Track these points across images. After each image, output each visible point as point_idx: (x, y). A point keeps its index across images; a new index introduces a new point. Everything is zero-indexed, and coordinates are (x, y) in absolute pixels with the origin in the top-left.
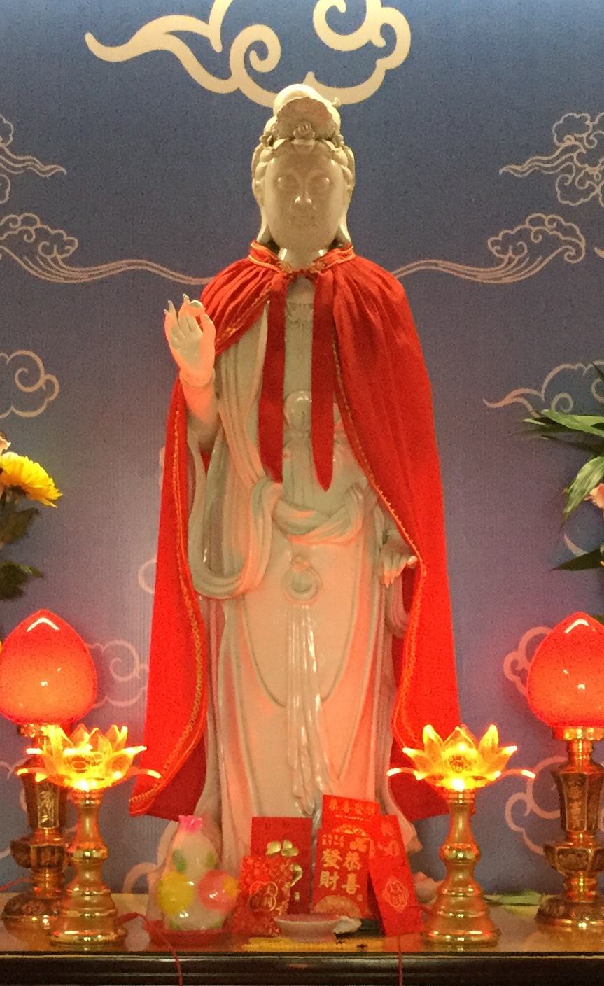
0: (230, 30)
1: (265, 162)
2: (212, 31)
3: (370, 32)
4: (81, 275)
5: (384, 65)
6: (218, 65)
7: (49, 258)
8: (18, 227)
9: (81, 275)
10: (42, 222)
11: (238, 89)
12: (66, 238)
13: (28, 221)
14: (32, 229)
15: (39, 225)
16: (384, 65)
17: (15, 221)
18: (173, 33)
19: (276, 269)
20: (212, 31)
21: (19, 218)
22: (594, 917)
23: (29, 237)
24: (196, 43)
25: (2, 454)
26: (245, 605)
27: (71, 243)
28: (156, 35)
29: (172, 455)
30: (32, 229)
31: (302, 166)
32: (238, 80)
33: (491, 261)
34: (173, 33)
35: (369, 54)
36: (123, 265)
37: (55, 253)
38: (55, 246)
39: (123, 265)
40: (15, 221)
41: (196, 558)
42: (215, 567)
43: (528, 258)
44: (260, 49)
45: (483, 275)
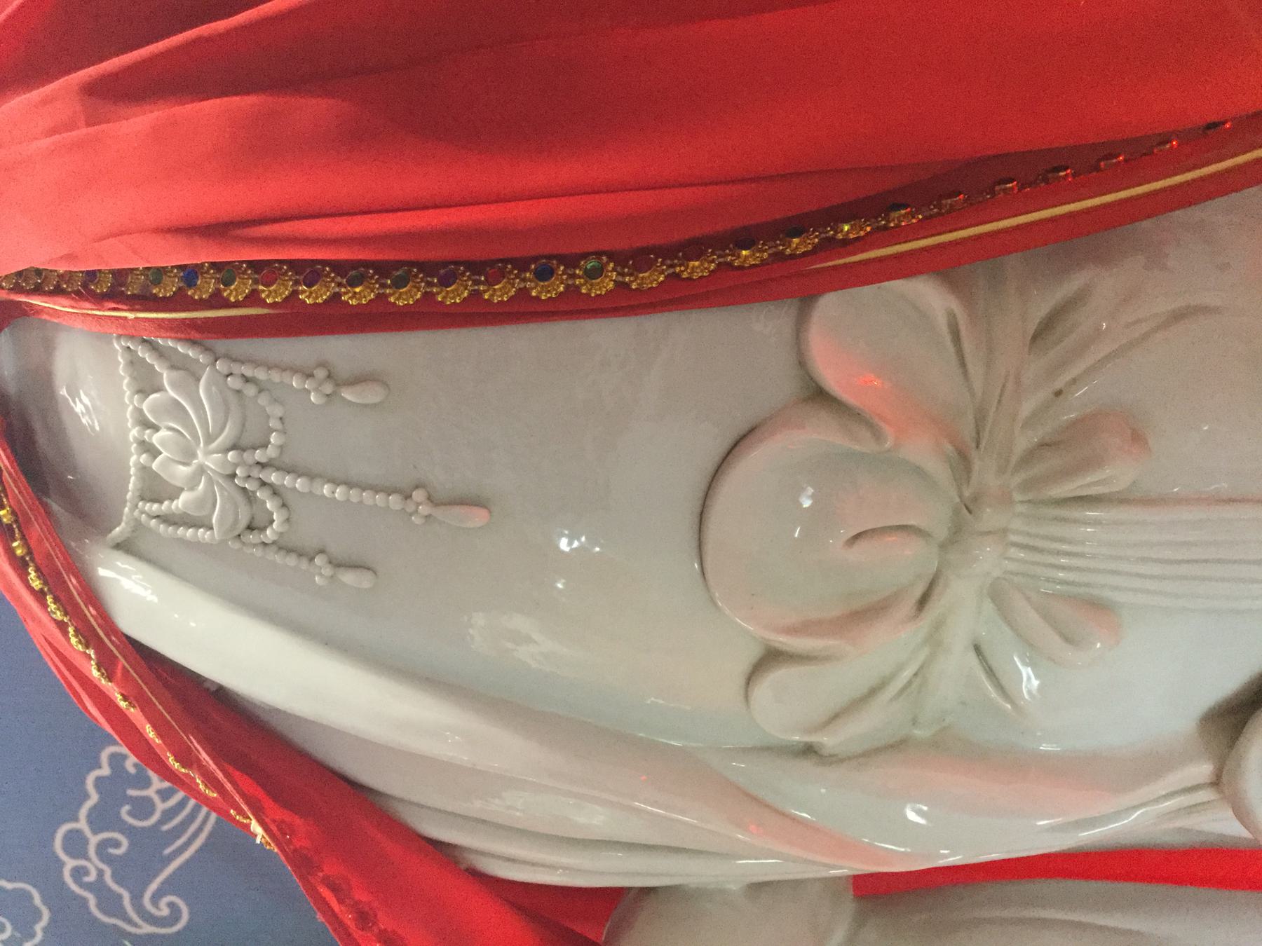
7: (161, 806)
8: (93, 865)
10: (62, 865)
12: (105, 771)
13: (75, 844)
14: (94, 840)
15: (82, 825)
17: (78, 873)
18: (747, 697)
19: (213, 445)
21: (70, 863)
22: (803, 489)
23: (117, 844)
26: (401, 800)
27: (116, 760)
29: (797, 234)
30: (94, 840)
34: (747, 697)
37: (150, 792)
38: (132, 792)
40: (78, 873)
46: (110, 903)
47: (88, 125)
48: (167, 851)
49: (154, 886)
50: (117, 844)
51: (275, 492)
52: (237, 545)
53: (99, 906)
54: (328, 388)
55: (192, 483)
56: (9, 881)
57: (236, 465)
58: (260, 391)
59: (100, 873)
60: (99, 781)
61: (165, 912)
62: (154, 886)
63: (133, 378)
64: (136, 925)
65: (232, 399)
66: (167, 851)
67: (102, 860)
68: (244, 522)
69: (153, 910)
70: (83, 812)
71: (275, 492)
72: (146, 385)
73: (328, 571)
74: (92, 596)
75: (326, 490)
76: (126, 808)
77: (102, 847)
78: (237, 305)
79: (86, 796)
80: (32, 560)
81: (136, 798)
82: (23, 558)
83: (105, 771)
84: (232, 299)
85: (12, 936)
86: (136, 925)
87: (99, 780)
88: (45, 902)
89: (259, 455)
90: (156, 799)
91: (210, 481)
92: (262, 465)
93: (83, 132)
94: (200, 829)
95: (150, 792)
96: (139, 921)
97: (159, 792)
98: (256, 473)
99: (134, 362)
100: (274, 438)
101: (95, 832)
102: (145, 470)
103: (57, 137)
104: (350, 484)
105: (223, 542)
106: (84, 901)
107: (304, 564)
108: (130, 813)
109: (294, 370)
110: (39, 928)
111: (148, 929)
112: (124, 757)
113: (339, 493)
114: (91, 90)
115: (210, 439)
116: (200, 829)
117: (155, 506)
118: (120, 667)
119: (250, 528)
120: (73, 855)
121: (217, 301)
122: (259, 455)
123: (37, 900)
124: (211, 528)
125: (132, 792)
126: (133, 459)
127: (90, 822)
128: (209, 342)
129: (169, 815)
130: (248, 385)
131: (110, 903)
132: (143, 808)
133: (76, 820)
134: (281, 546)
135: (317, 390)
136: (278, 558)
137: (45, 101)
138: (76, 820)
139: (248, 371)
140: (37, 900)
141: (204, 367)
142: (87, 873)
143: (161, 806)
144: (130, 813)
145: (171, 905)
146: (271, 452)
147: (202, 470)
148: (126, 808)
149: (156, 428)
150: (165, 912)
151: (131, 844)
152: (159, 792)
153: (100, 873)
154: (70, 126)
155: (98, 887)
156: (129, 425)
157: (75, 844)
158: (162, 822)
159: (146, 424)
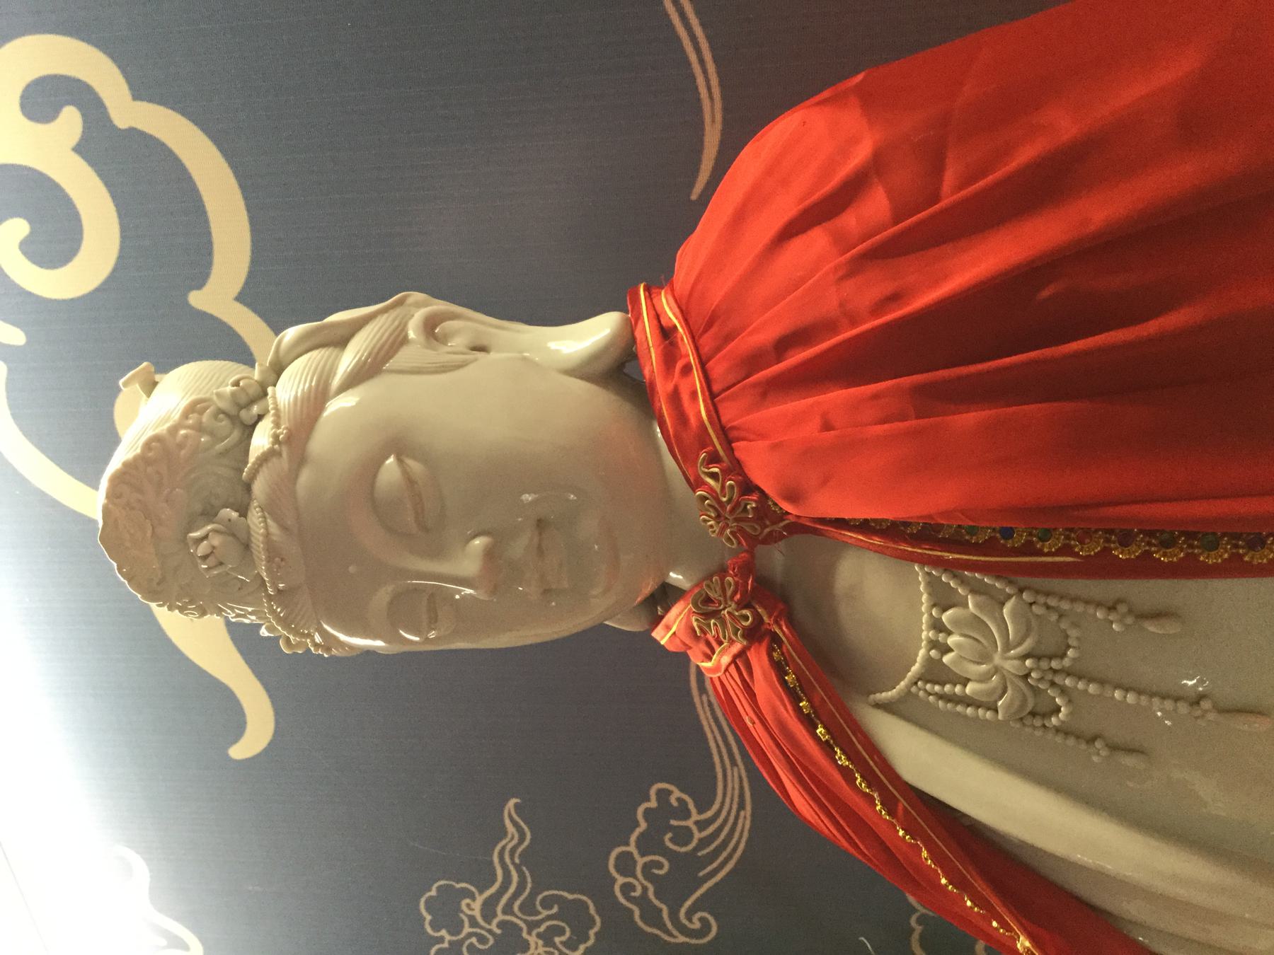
7: (697, 835)
8: (640, 883)
10: (614, 880)
12: (653, 804)
13: (626, 865)
14: (641, 861)
15: (632, 848)
17: (627, 889)
21: (621, 880)
23: (660, 866)
30: (641, 861)
37: (689, 823)
38: (673, 822)
40: (627, 889)
46: (652, 916)
47: (917, 418)
48: (701, 874)
49: (688, 903)
50: (660, 866)
51: (1063, 691)
52: (1018, 725)
53: (642, 917)
54: (1129, 620)
55: (984, 678)
56: (569, 892)
57: (1031, 670)
58: (1061, 616)
59: (645, 889)
60: (648, 812)
61: (697, 925)
62: (688, 903)
63: (930, 594)
64: (671, 935)
65: (1034, 623)
66: (701, 874)
67: (646, 878)
68: (1030, 707)
69: (685, 922)
70: (633, 838)
71: (1063, 691)
72: (943, 601)
73: (1104, 753)
74: (874, 750)
75: (1118, 694)
76: (669, 835)
77: (647, 868)
78: (1049, 554)
79: (637, 825)
80: (818, 717)
81: (678, 827)
82: (808, 715)
83: (653, 804)
84: (1046, 550)
85: (570, 938)
86: (671, 935)
87: (647, 811)
88: (598, 911)
89: (1055, 664)
90: (694, 829)
91: (1004, 678)
92: (1055, 671)
93: (913, 423)
94: (730, 857)
95: (689, 823)
96: (675, 932)
97: (697, 823)
98: (1049, 676)
99: (933, 584)
100: (1070, 653)
101: (643, 855)
102: (929, 661)
103: (886, 426)
104: (1140, 692)
105: (1006, 722)
106: (631, 912)
107: (1083, 746)
108: (671, 840)
109: (1099, 605)
110: (592, 933)
111: (682, 939)
112: (670, 793)
113: (1131, 698)
114: (919, 391)
115: (1008, 646)
116: (730, 857)
117: (937, 688)
118: (900, 807)
119: (1033, 714)
120: (623, 873)
121: (1029, 549)
122: (1055, 664)
123: (592, 910)
124: (996, 711)
125: (673, 822)
126: (922, 652)
127: (638, 846)
128: (1013, 578)
129: (704, 843)
130: (1202, 703)
131: (652, 916)
132: (683, 836)
133: (627, 844)
134: (1061, 730)
135: (1120, 621)
136: (1059, 739)
137: (876, 396)
138: (627, 844)
139: (1052, 602)
140: (592, 910)
141: (1009, 597)
142: (633, 888)
143: (697, 835)
144: (671, 840)
145: (701, 919)
146: (1066, 662)
147: (997, 670)
148: (669, 835)
149: (949, 633)
150: (697, 925)
151: (671, 868)
152: (697, 823)
153: (645, 889)
154: (903, 418)
155: (643, 901)
156: (924, 627)
157: (626, 865)
158: (696, 849)
159: (938, 626)
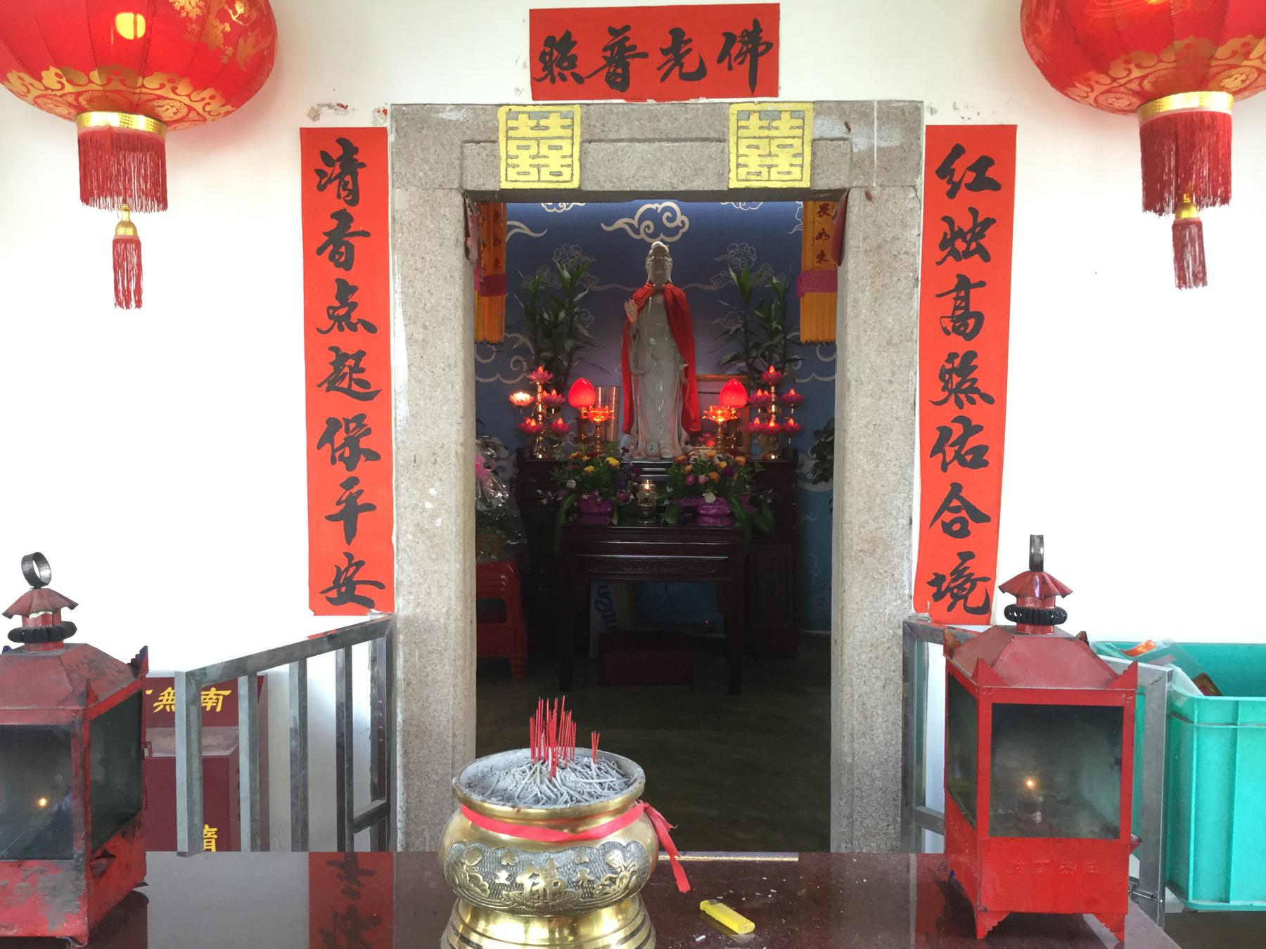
0: (640, 222)
1: (649, 261)
2: (635, 222)
3: (678, 222)
4: (600, 288)
5: (682, 231)
6: (637, 231)
9: (600, 288)
11: (532, 12)
16: (682, 231)
20: (635, 222)
24: (631, 225)
25: (144, 651)
28: (620, 223)
31: (659, 264)
32: (643, 236)
33: (709, 283)
35: (678, 228)
36: (610, 286)
39: (610, 286)
41: (632, 364)
42: (637, 366)
43: (331, 247)
44: (648, 227)
45: (708, 288)
